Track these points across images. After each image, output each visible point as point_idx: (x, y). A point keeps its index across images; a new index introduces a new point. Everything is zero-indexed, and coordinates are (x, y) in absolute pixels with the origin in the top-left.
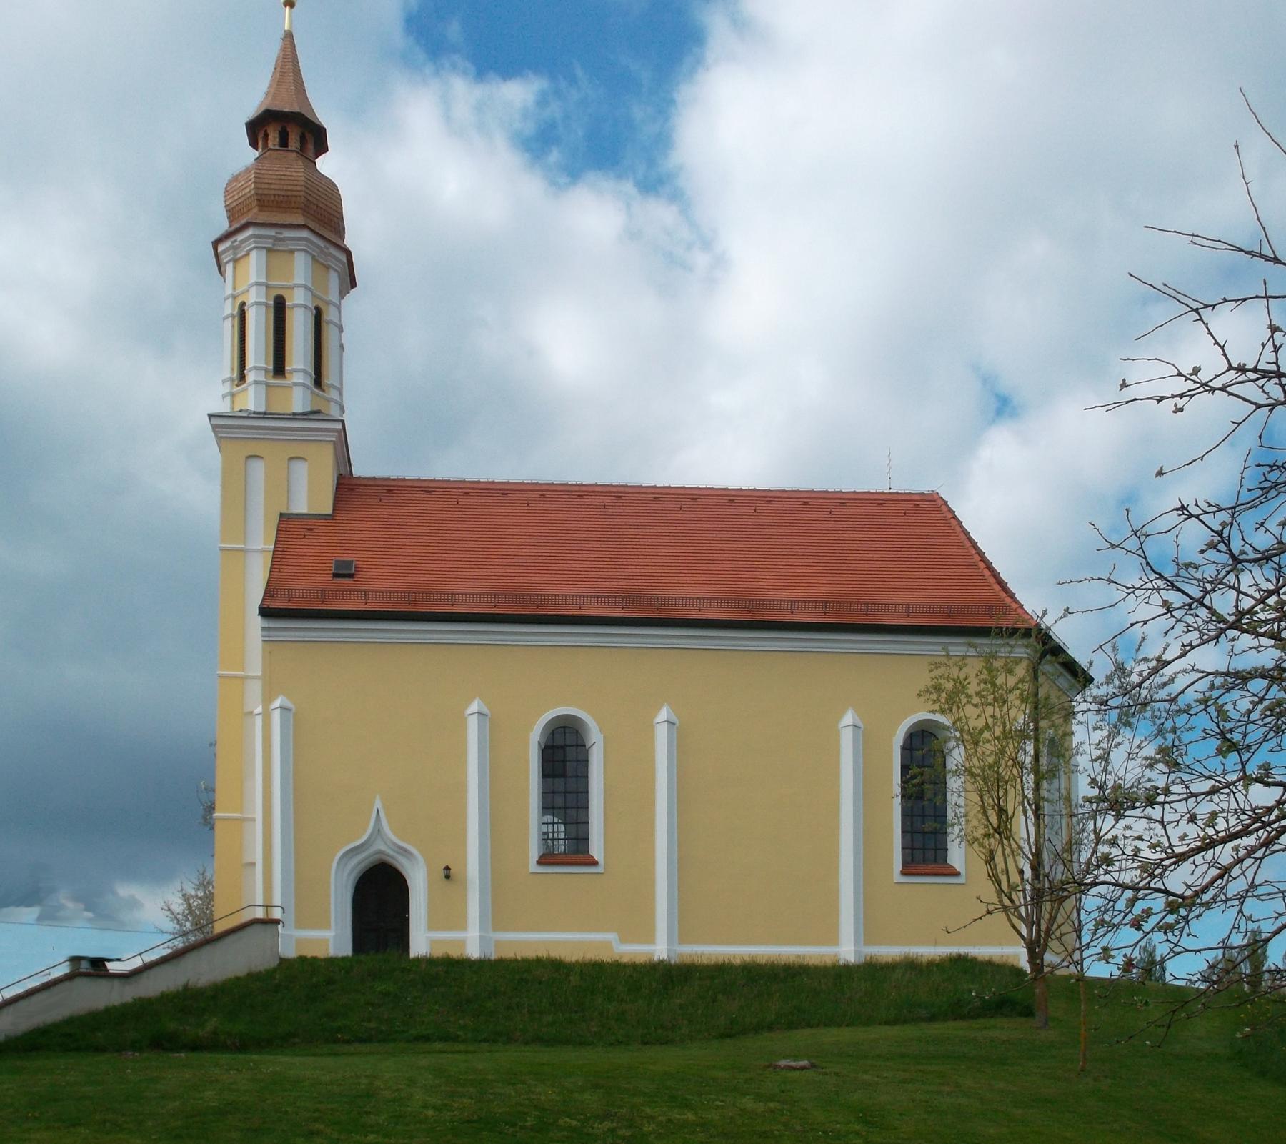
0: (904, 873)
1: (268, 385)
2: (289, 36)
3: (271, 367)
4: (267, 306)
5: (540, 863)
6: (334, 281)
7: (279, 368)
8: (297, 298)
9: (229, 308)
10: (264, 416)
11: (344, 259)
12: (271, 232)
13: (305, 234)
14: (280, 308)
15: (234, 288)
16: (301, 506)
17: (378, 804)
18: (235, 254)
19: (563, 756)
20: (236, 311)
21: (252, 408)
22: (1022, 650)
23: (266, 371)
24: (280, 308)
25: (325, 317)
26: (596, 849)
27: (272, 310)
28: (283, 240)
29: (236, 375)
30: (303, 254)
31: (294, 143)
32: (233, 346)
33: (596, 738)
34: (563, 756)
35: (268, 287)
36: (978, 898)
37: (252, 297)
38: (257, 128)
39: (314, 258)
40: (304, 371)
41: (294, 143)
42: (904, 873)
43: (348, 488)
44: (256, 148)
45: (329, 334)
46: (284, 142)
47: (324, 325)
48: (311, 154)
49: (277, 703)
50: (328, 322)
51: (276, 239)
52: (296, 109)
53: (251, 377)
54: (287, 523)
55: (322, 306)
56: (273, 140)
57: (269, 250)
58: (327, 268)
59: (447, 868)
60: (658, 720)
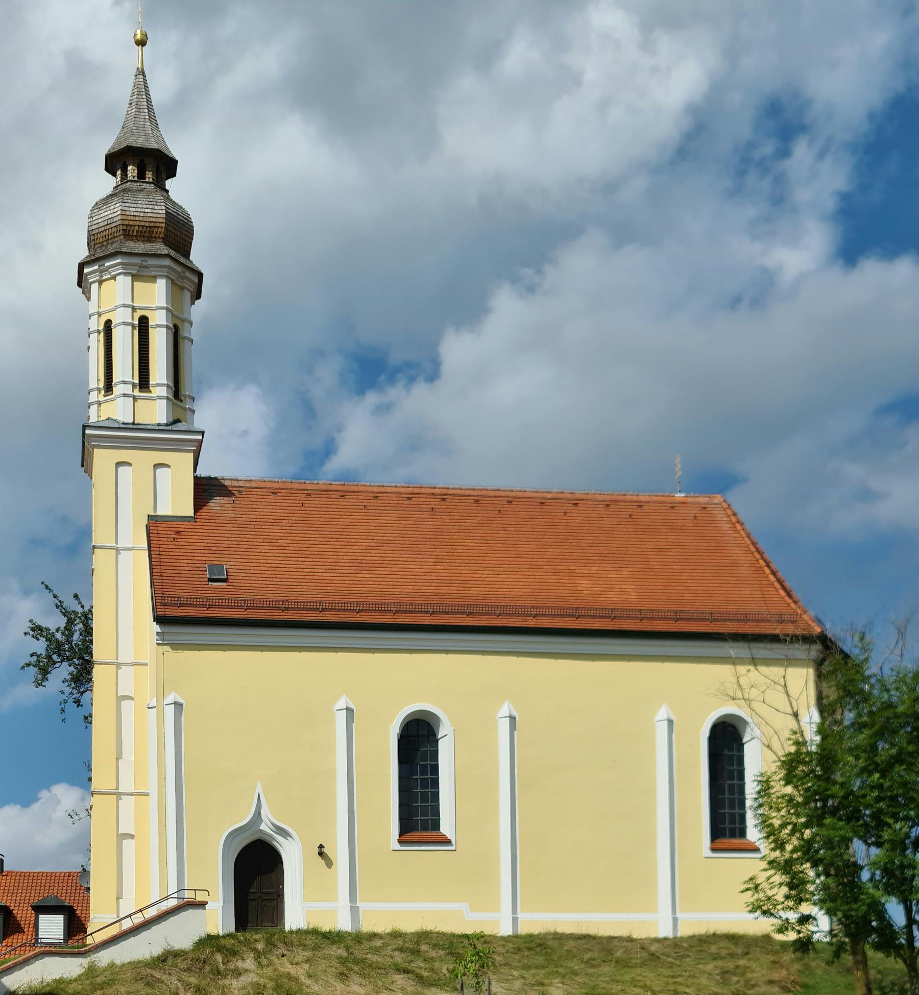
1: (135, 399)
3: (137, 381)
6: (187, 296)
7: (144, 383)
8: (158, 319)
10: (126, 427)
11: (196, 281)
12: (137, 260)
13: (167, 262)
14: (143, 326)
15: (99, 307)
16: (164, 510)
17: (259, 789)
19: (418, 741)
20: (101, 327)
21: (121, 419)
24: (143, 326)
25: (183, 333)
26: (446, 828)
28: (147, 267)
29: (102, 385)
31: (149, 176)
34: (418, 741)
35: (134, 309)
37: (117, 317)
38: (115, 162)
39: (173, 282)
43: (206, 489)
44: (114, 175)
45: (184, 346)
46: (141, 176)
47: (181, 341)
49: (170, 699)
50: (184, 338)
51: (141, 267)
52: (154, 145)
53: (118, 390)
54: (156, 527)
55: (179, 324)
56: (132, 171)
57: (133, 276)
58: (182, 288)
59: (321, 846)
60: (658, 717)
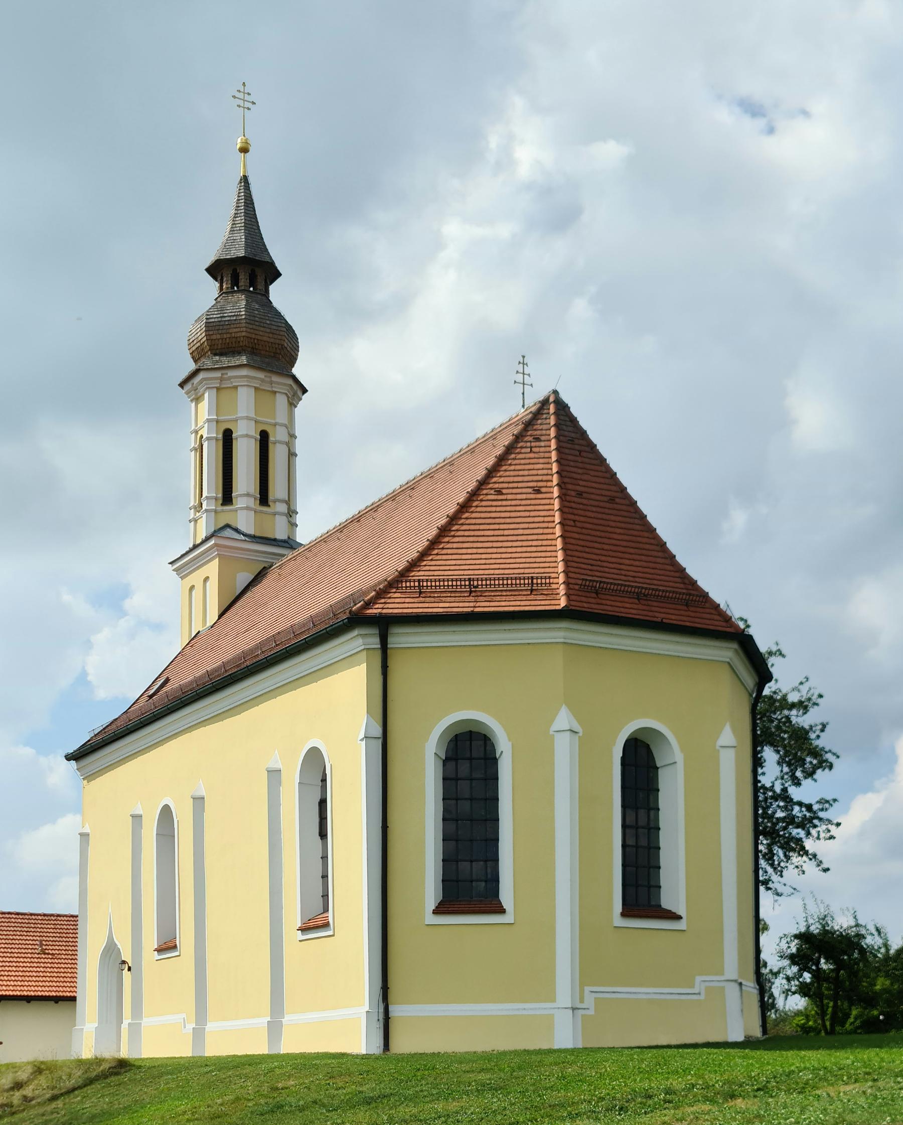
0: (627, 913)
1: (216, 511)
2: (245, 180)
3: (220, 495)
4: (217, 439)
5: (437, 911)
9: (193, 443)
12: (218, 374)
13: (244, 372)
14: (228, 438)
18: (196, 394)
22: (726, 652)
23: (216, 499)
27: (221, 443)
28: (230, 378)
30: (245, 389)
31: (243, 280)
32: (217, 455)
33: (504, 746)
35: (217, 421)
36: (838, 757)
40: (248, 495)
41: (243, 280)
42: (624, 914)
48: (261, 286)
